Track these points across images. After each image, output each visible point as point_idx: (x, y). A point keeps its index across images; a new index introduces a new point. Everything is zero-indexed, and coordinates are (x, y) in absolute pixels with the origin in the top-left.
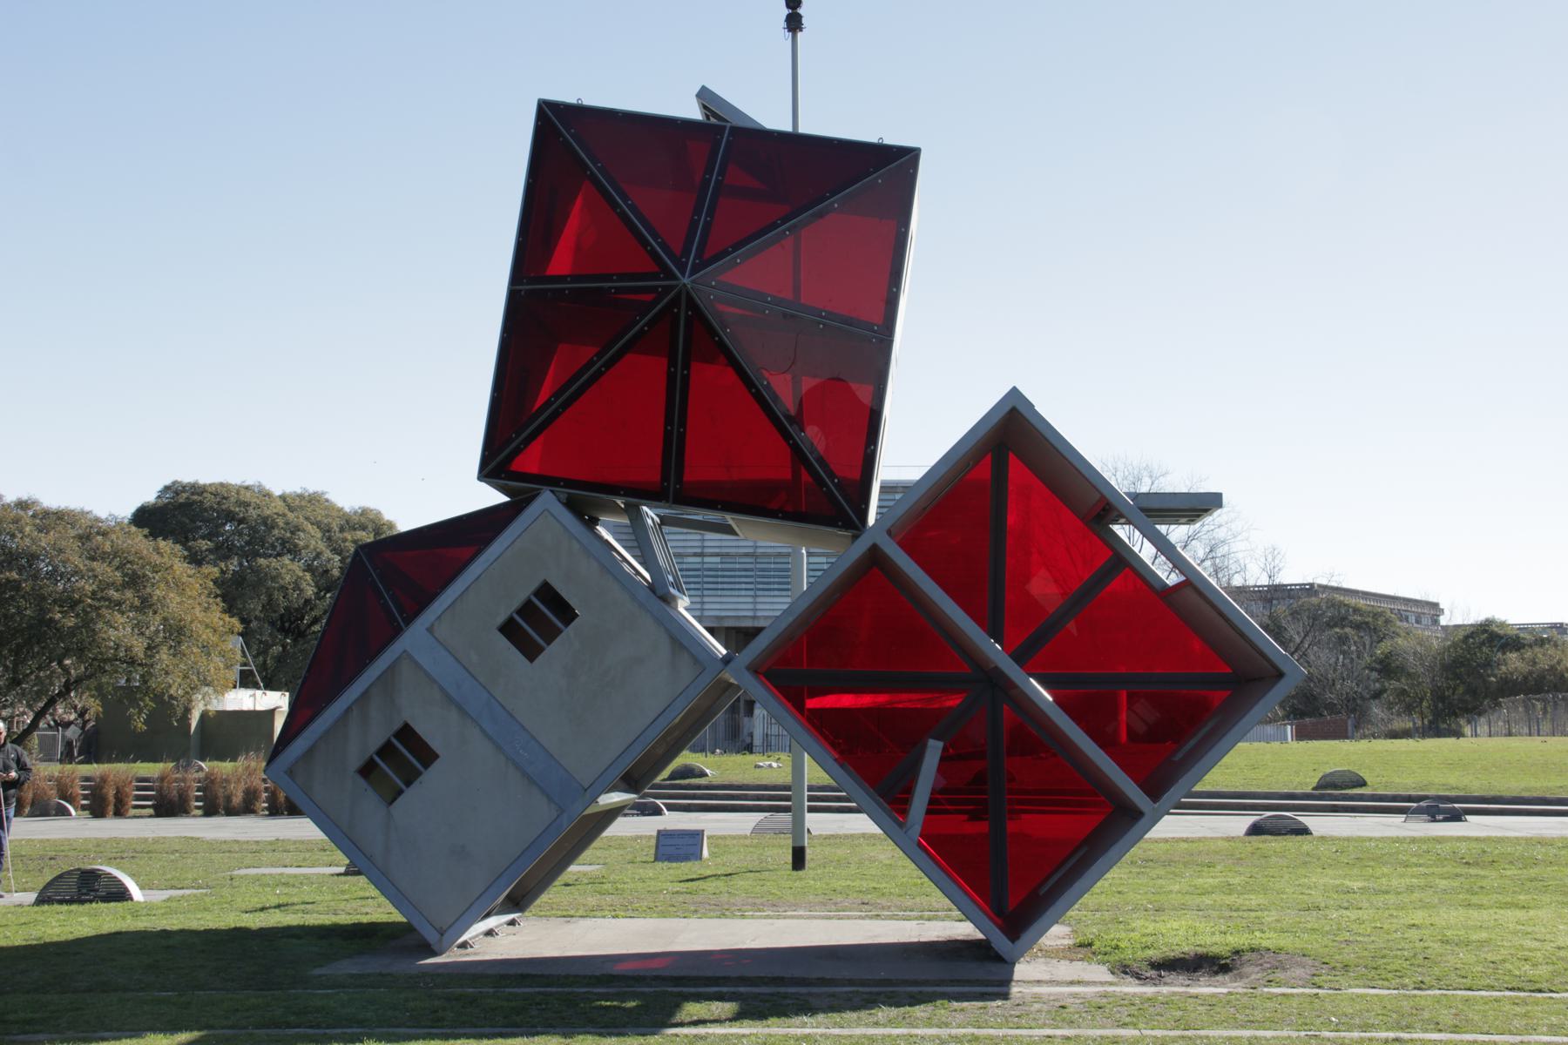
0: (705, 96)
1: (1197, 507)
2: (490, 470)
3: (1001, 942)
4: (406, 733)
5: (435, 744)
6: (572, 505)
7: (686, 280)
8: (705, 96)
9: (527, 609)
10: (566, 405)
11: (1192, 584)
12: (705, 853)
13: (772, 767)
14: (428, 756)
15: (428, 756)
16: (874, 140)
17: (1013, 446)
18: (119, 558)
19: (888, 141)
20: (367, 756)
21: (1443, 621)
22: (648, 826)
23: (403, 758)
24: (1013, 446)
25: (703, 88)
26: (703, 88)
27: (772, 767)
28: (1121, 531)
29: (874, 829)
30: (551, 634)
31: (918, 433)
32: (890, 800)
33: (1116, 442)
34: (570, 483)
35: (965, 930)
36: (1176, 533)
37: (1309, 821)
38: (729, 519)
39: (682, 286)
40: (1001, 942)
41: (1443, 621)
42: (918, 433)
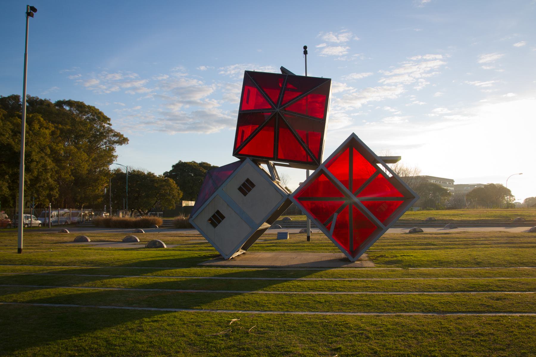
0: (282, 69)
1: (394, 160)
2: (235, 154)
3: (351, 258)
4: (218, 212)
5: (224, 215)
6: (254, 161)
7: (278, 110)
8: (282, 69)
9: (244, 185)
10: (251, 139)
11: (395, 176)
12: (288, 238)
13: (303, 218)
14: (223, 217)
15: (223, 217)
16: (320, 77)
17: (353, 146)
18: (164, 181)
19: (324, 77)
20: (220, 224)
21: (455, 183)
22: (276, 231)
23: (217, 219)
24: (353, 146)
25: (245, 196)
26: (245, 196)
27: (303, 218)
28: (380, 165)
29: (321, 232)
30: (249, 190)
31: (331, 143)
32: (326, 227)
33: (377, 144)
34: (252, 156)
35: (343, 255)
36: (390, 165)
37: (423, 229)
38: (177, 310)
39: (278, 112)
40: (351, 258)
41: (455, 183)
42: (331, 143)
